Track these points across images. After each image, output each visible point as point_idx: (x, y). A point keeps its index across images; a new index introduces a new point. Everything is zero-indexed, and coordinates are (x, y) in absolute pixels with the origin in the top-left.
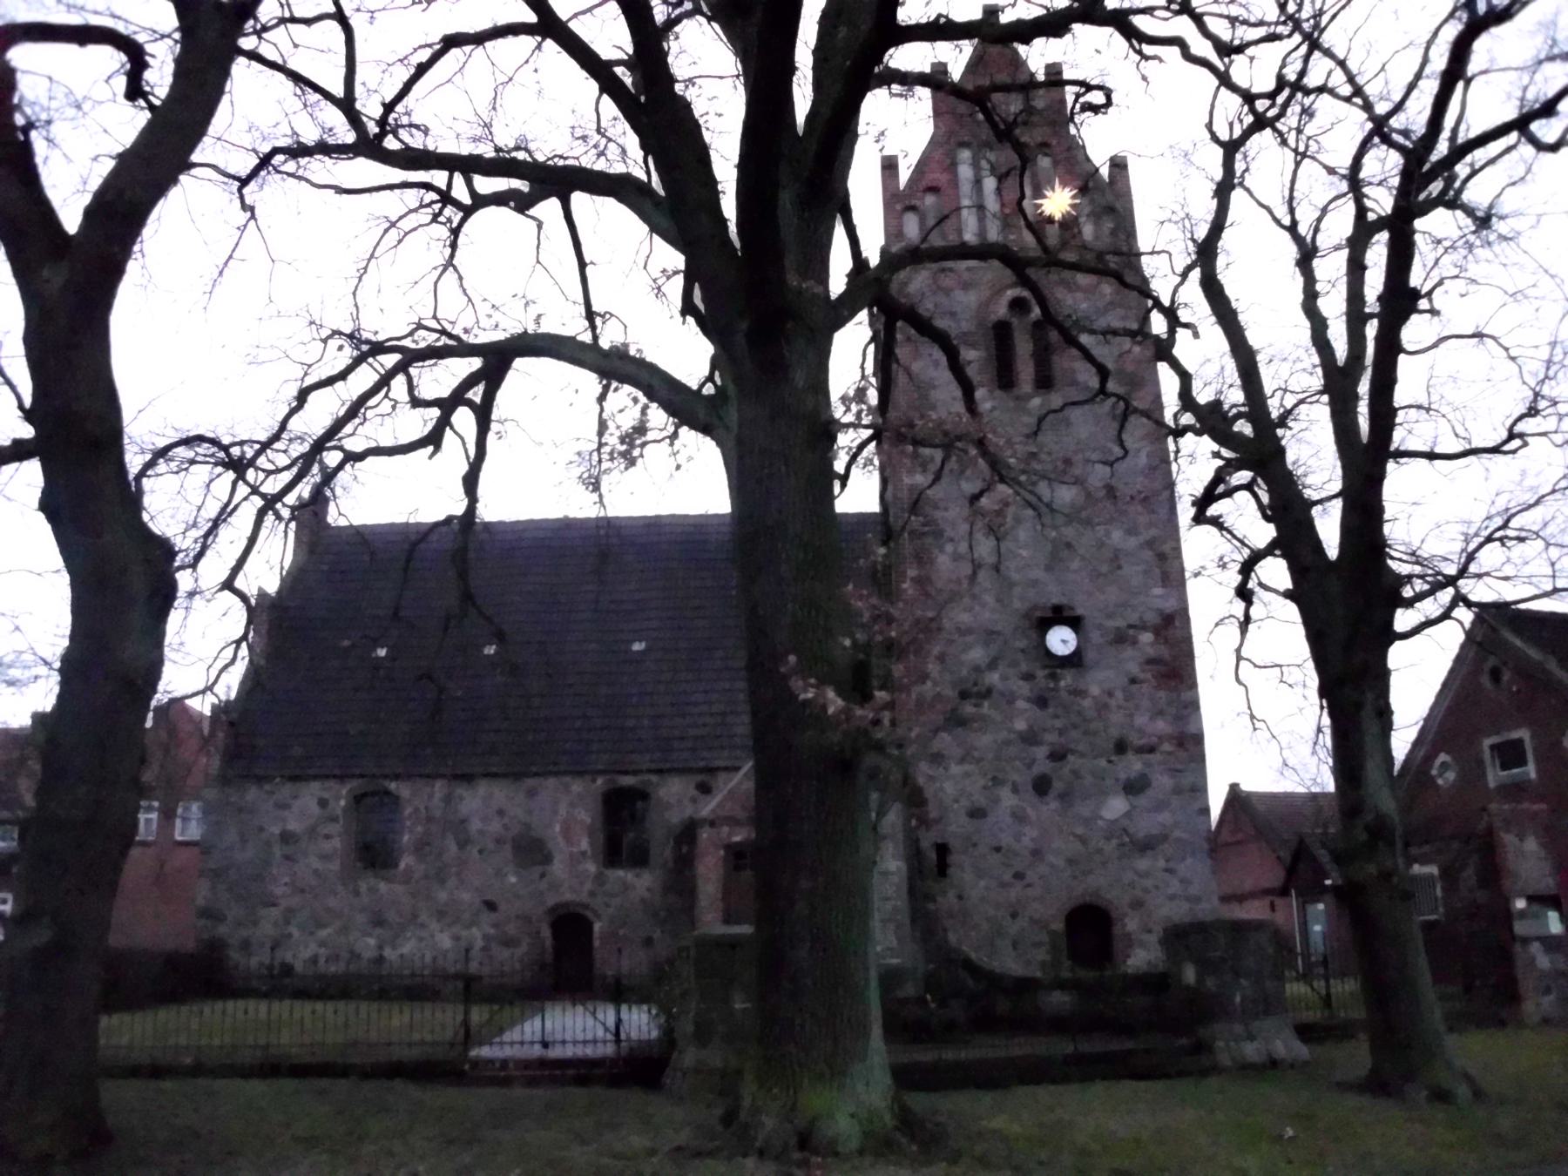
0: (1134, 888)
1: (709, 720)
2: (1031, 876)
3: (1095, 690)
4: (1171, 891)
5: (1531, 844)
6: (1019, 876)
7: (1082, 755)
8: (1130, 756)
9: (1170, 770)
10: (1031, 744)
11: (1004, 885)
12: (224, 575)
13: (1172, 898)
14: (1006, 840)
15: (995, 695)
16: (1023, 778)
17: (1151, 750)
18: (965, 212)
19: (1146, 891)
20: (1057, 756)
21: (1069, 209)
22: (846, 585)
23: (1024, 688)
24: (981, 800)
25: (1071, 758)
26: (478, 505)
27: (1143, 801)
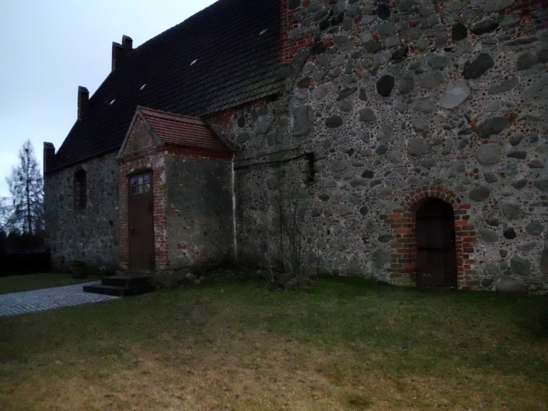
0: (477, 178)
2: (378, 173)
4: (520, 177)
6: (368, 174)
9: (512, 44)
10: (375, 52)
11: (355, 184)
13: (520, 185)
14: (356, 142)
15: (346, 18)
17: (493, 27)
18: (324, 19)
19: (490, 179)
22: (45, 227)
24: (335, 110)
25: (410, 54)
27: (484, 83)
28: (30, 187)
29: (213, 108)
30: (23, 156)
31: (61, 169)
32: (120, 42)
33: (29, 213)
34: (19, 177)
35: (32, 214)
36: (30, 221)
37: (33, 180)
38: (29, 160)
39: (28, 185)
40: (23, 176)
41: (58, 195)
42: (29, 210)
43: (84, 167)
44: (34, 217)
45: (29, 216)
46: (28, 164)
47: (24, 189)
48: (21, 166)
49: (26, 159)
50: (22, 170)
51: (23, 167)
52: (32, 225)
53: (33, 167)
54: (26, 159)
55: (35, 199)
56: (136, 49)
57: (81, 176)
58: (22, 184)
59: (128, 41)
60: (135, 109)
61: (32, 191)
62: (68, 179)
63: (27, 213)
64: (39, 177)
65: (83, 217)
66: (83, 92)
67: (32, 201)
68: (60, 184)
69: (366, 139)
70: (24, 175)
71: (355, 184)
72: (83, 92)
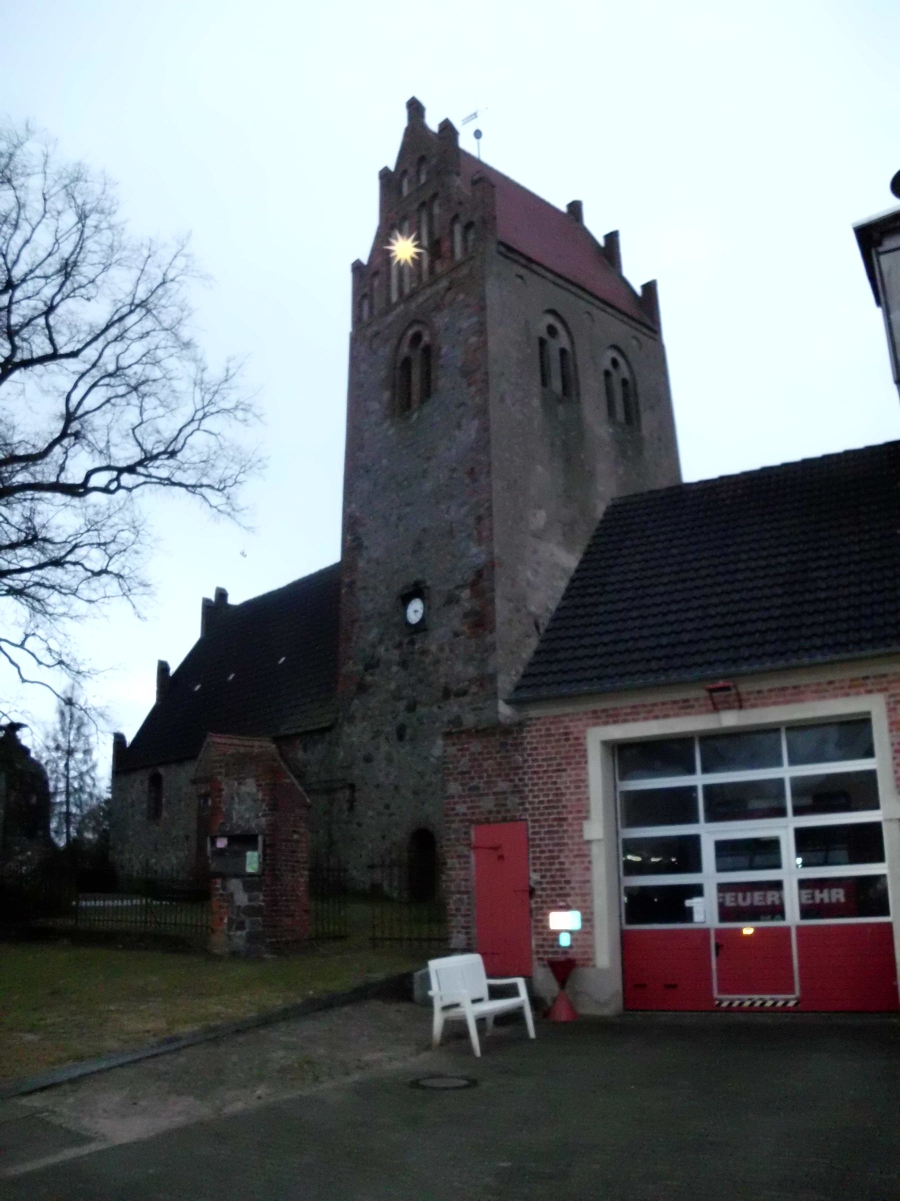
1: (659, 546)
3: (434, 648)
5: (250, 786)
6: (387, 807)
7: (425, 705)
8: (452, 700)
12: (19, 649)
16: (390, 729)
17: (465, 693)
20: (411, 708)
21: (410, 261)
23: (395, 655)
26: (391, 162)
28: (72, 764)
29: (283, 731)
30: (63, 709)
31: (134, 770)
32: (212, 597)
33: (68, 808)
34: (52, 744)
35: (74, 810)
36: (68, 823)
37: (77, 751)
38: (72, 716)
39: (68, 760)
40: (60, 743)
41: (129, 801)
42: (67, 803)
43: (161, 770)
44: (75, 815)
45: (68, 814)
46: (71, 723)
47: (62, 764)
48: (58, 726)
49: (67, 715)
50: (61, 733)
51: (62, 729)
52: (71, 829)
53: (78, 729)
54: (67, 715)
55: (79, 784)
56: (235, 606)
57: (156, 781)
58: (60, 758)
59: (222, 595)
60: (205, 737)
61: (74, 769)
62: (142, 782)
63: (64, 809)
64: (87, 747)
65: (157, 828)
66: (163, 668)
67: (73, 787)
68: (132, 786)
69: (387, 775)
70: (61, 739)
71: (379, 814)
72: (163, 668)
